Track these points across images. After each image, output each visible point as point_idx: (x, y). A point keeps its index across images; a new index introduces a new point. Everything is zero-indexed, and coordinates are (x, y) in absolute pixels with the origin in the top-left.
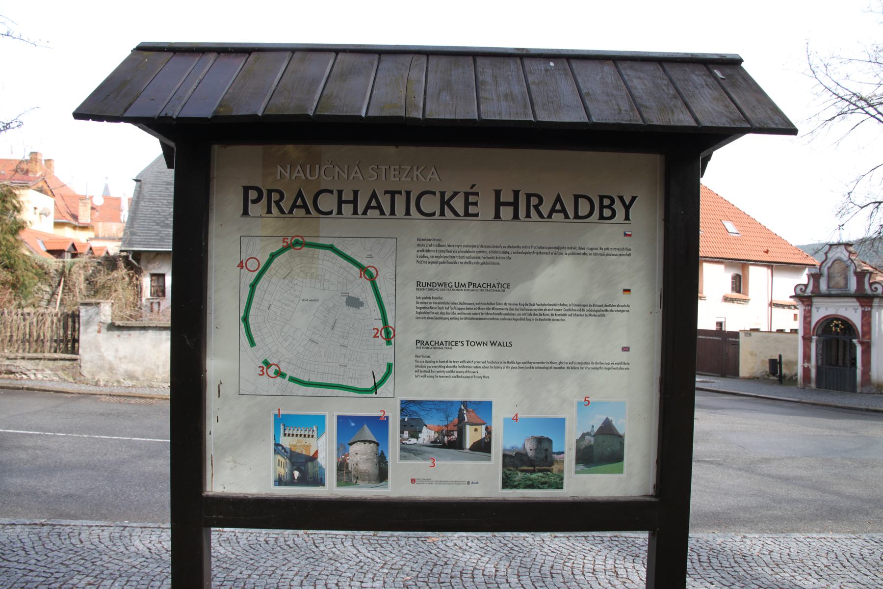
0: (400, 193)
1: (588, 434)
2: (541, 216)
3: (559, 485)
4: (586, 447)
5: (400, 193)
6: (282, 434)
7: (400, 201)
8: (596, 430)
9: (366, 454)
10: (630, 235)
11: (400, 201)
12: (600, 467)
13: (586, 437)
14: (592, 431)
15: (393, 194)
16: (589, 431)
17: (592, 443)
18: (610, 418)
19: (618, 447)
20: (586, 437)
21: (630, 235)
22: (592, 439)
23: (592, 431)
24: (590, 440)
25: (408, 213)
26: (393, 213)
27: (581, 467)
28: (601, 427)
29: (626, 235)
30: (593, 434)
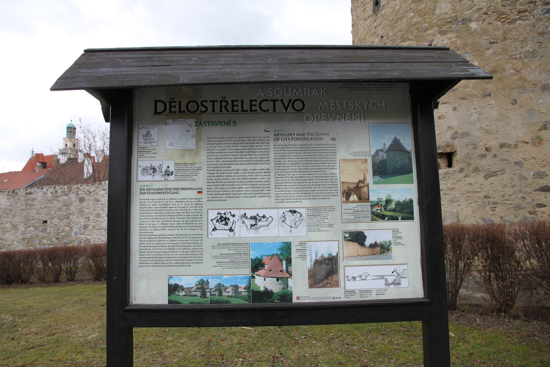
0: (217, 101)
1: (381, 150)
2: (227, 111)
3: (411, 201)
4: (380, 162)
5: (217, 101)
6: (205, 191)
7: (217, 105)
8: (387, 147)
9: (484, 221)
10: (269, 131)
11: (217, 105)
12: (393, 178)
13: (380, 153)
14: (384, 148)
15: (213, 102)
16: (382, 147)
17: (385, 158)
18: (398, 137)
19: (407, 161)
20: (380, 153)
21: (269, 131)
22: (385, 155)
23: (384, 148)
24: (383, 156)
25: (221, 111)
26: (213, 111)
27: (378, 178)
28: (391, 145)
29: (266, 131)
30: (385, 150)
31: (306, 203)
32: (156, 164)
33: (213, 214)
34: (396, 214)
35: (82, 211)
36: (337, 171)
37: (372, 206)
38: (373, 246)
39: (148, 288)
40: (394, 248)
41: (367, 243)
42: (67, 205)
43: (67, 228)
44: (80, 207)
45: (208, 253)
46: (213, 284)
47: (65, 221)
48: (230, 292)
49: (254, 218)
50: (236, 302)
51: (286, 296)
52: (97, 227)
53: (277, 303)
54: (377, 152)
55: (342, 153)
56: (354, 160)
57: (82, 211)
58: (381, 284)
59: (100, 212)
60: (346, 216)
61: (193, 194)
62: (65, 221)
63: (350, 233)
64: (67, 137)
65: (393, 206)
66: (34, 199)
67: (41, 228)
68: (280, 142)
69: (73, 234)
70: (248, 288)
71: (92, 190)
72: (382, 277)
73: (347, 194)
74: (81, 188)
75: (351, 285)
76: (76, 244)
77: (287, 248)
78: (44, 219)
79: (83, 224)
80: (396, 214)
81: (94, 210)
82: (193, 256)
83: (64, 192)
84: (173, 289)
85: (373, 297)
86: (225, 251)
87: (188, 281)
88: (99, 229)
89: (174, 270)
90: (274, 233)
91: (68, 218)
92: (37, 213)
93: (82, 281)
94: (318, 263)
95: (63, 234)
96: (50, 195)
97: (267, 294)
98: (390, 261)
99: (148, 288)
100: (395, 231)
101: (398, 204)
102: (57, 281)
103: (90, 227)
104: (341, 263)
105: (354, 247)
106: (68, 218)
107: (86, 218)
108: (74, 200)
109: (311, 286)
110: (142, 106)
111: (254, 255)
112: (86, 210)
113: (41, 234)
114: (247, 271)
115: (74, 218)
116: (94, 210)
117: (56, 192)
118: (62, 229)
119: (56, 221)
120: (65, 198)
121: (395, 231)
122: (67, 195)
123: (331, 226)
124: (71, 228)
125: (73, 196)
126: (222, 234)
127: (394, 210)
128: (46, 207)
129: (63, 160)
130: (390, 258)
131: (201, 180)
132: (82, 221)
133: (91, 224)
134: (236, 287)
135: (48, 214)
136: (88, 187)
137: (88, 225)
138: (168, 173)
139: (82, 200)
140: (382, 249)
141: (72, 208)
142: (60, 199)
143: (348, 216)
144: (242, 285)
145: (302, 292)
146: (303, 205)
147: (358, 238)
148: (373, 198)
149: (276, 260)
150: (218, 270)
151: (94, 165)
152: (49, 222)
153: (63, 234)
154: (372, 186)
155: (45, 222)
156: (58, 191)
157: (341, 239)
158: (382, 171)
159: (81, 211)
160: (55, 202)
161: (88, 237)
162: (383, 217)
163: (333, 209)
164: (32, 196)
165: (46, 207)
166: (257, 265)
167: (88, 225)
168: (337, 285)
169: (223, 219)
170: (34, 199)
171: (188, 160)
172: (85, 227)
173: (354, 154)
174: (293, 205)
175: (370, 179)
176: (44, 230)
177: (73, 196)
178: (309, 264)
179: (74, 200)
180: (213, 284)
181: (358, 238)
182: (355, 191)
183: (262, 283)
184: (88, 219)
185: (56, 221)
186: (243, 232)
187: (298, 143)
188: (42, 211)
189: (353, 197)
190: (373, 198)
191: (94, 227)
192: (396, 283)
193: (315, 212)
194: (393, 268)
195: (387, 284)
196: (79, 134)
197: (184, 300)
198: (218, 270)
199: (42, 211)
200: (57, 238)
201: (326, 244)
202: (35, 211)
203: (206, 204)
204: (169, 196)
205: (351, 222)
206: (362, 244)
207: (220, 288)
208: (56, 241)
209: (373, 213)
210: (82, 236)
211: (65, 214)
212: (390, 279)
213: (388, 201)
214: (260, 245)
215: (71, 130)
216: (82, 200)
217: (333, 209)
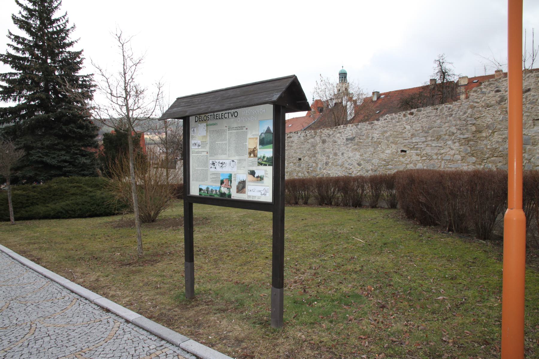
24: (263, 135)
27: (261, 146)
31: (237, 158)
32: (196, 142)
33: (211, 162)
34: (266, 163)
35: (324, 151)
36: (247, 143)
37: (258, 159)
38: (258, 177)
39: (194, 191)
40: (265, 178)
41: (256, 176)
42: (314, 146)
43: (314, 165)
44: (322, 147)
45: (210, 177)
46: (210, 189)
47: (313, 159)
48: (214, 192)
49: (222, 163)
50: (216, 196)
51: (230, 196)
52: (335, 164)
53: (227, 198)
54: (262, 134)
55: (249, 136)
56: (253, 138)
57: (324, 151)
58: (259, 194)
59: (337, 151)
60: (250, 164)
61: (205, 154)
62: (313, 159)
63: (250, 171)
64: (340, 83)
65: (265, 159)
66: (292, 142)
67: (297, 164)
68: (230, 131)
69: (318, 170)
70: (219, 191)
71: (331, 133)
72: (260, 191)
73: (250, 154)
74: (323, 132)
75: (250, 193)
76: (320, 176)
77: (231, 176)
78: (299, 157)
79: (325, 161)
80: (266, 163)
81: (333, 150)
82: (205, 179)
83: (311, 135)
84: (200, 190)
85: (256, 199)
86: (214, 176)
87: (204, 188)
88: (337, 166)
89: (201, 183)
90: (228, 170)
91: (315, 156)
92: (295, 153)
93: (311, 204)
94: (239, 183)
95: (311, 169)
96: (302, 138)
97: (224, 194)
98: (263, 185)
99: (194, 191)
100: (266, 171)
101: (267, 158)
102: (296, 203)
103: (330, 164)
104: (247, 184)
105: (251, 176)
106: (315, 156)
107: (327, 156)
108: (318, 141)
109: (237, 192)
110: (192, 119)
111: (221, 178)
112: (327, 150)
113: (297, 169)
114: (220, 184)
115: (319, 156)
116: (333, 150)
117: (306, 135)
118: (311, 165)
119: (307, 158)
120: (313, 140)
121: (266, 171)
122: (313, 138)
123: (244, 167)
124: (317, 164)
125: (318, 139)
126: (213, 170)
127: (266, 161)
128: (300, 148)
129: (332, 104)
130: (263, 183)
131: (207, 149)
132: (324, 159)
133: (331, 161)
134: (216, 190)
135: (301, 153)
136: (328, 131)
137: (329, 162)
138: (199, 146)
139: (324, 142)
140: (260, 178)
141: (318, 148)
142: (309, 141)
143: (251, 163)
144: (218, 190)
145: (235, 196)
146: (236, 158)
147: (252, 173)
148: (259, 156)
149: (227, 181)
150: (211, 184)
151: (356, 106)
152: (302, 160)
153: (311, 169)
154: (259, 150)
155: (300, 159)
156: (308, 135)
157: (247, 173)
158: (263, 143)
159: (324, 151)
160: (305, 143)
161: (329, 172)
162: (261, 164)
163: (245, 160)
164: (291, 139)
165: (300, 148)
166: (222, 182)
167: (329, 162)
168: (245, 193)
169: (213, 164)
170: (292, 142)
171: (204, 140)
172: (327, 164)
173: (253, 135)
174: (233, 158)
175: (258, 147)
176: (300, 166)
177: (318, 139)
178: (237, 183)
179: (318, 141)
180: (210, 189)
181: (252, 173)
182: (253, 152)
183: (224, 190)
184: (328, 157)
185: (307, 158)
186: (219, 169)
187: (235, 131)
188: (297, 151)
189: (252, 155)
190: (259, 156)
191: (333, 163)
192: (265, 194)
193: (240, 161)
194: (264, 187)
195: (262, 195)
196: (349, 78)
197: (204, 195)
198: (211, 184)
199: (297, 151)
200: (308, 172)
201: (242, 175)
202: (293, 151)
203: (209, 158)
204: (199, 154)
205: (250, 166)
206: (254, 176)
207: (212, 191)
208: (307, 174)
209: (258, 162)
210: (325, 171)
211: (313, 153)
212: (263, 192)
213: (264, 157)
214: (223, 174)
215: (343, 76)
216: (324, 142)
217: (245, 160)
